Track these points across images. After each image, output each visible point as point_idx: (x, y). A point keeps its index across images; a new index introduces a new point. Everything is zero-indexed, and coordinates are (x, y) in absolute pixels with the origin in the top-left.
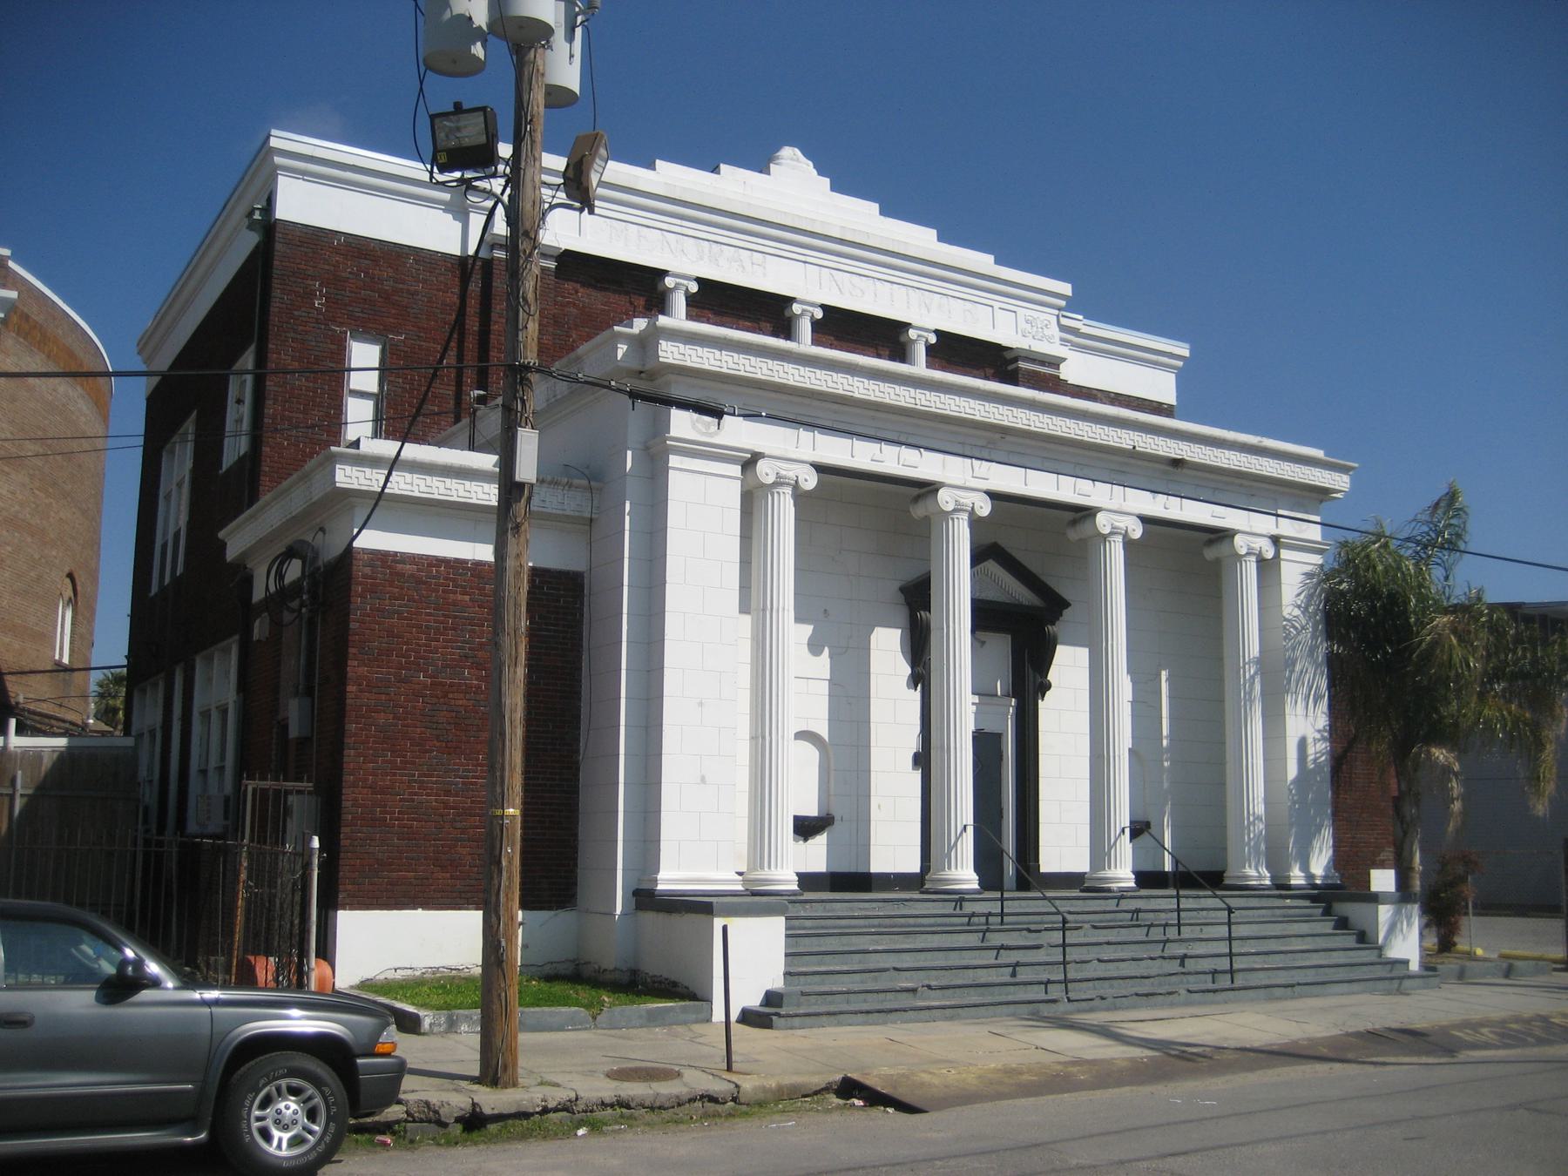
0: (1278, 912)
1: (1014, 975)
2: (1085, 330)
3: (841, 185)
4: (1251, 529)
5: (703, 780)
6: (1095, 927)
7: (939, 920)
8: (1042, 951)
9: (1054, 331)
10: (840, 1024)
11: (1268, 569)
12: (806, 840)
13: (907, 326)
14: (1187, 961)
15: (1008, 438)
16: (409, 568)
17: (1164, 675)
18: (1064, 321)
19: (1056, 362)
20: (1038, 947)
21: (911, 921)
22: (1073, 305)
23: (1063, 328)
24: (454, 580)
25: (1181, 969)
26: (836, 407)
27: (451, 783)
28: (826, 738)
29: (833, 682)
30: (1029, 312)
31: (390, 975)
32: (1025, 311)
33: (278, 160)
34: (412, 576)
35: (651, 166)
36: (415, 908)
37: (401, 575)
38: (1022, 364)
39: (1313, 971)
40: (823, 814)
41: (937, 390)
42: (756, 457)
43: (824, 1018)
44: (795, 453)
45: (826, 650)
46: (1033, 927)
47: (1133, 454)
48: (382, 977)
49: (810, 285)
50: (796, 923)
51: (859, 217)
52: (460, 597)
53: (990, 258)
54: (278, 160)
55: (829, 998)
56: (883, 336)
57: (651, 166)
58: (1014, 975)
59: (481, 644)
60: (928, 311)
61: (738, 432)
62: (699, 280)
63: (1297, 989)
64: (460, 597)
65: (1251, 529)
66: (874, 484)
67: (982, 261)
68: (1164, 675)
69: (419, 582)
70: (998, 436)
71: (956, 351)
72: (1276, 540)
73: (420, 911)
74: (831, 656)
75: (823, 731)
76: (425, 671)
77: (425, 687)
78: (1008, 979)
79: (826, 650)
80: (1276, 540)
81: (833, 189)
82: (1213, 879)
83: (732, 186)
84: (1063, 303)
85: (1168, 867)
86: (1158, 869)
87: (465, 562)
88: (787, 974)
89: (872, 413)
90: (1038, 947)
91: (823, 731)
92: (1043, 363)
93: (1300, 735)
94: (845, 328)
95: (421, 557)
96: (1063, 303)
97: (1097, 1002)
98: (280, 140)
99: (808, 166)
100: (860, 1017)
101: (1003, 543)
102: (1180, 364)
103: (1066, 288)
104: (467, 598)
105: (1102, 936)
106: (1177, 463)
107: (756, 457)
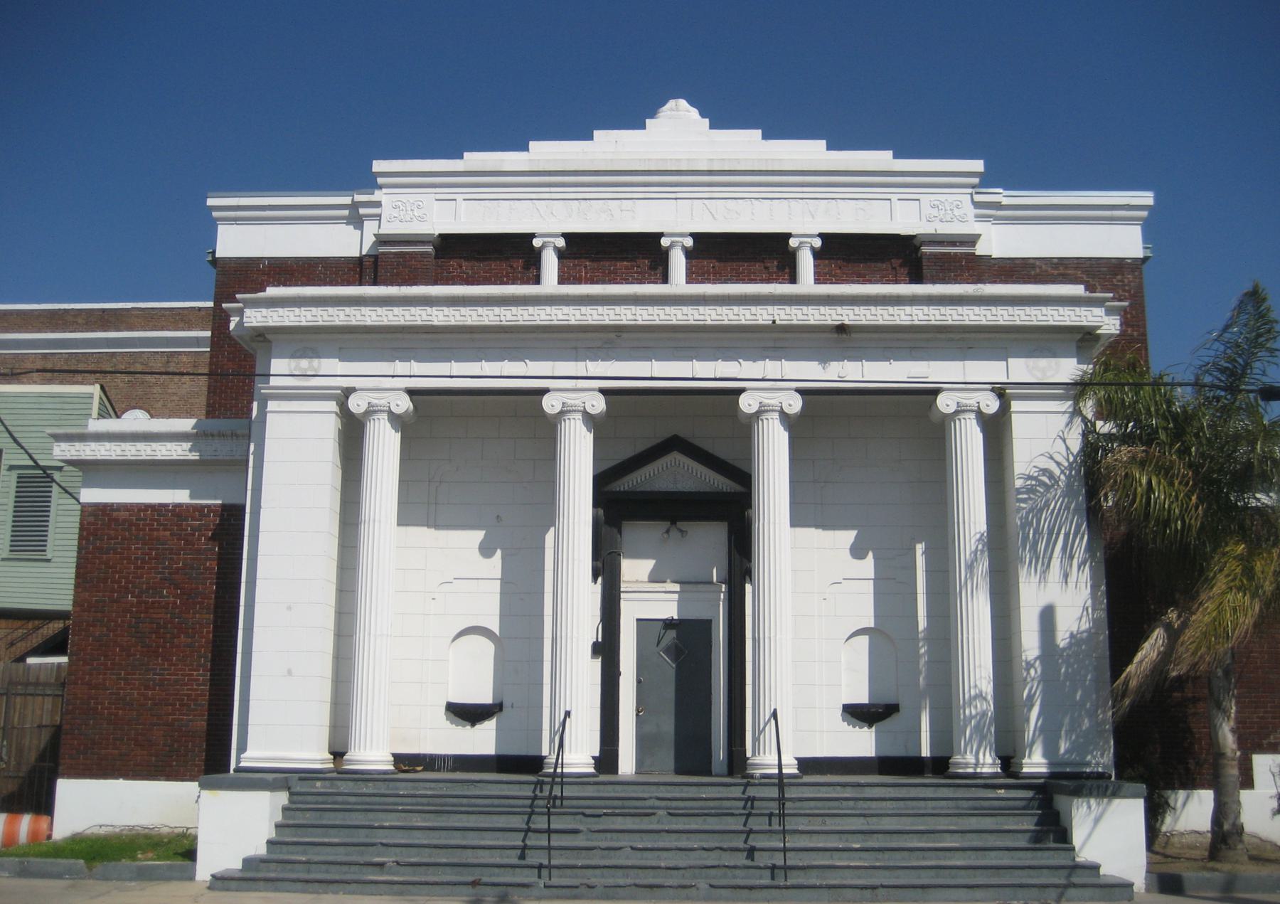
0: (965, 804)
1: (522, 857)
2: (1005, 201)
3: (718, 122)
4: (962, 383)
5: (290, 673)
6: (670, 814)
7: (496, 802)
8: (580, 836)
9: (971, 211)
10: (276, 890)
11: (996, 430)
12: (473, 725)
13: (789, 235)
14: (757, 854)
15: (625, 335)
16: (123, 515)
17: (920, 548)
18: (978, 198)
19: (972, 240)
20: (576, 832)
21: (465, 801)
22: (987, 180)
23: (977, 205)
24: (156, 520)
25: (749, 863)
26: (430, 336)
27: (149, 680)
28: (497, 631)
29: (504, 581)
30: (933, 197)
31: (96, 830)
32: (928, 197)
33: (215, 214)
34: (125, 520)
35: (525, 148)
36: (117, 778)
37: (116, 520)
38: (925, 249)
39: (932, 872)
40: (497, 702)
41: (525, 305)
42: (348, 392)
43: (262, 883)
44: (386, 385)
45: (499, 552)
46: (588, 811)
47: (774, 328)
48: (89, 832)
49: (676, 218)
50: (295, 798)
51: (745, 146)
52: (162, 533)
53: (889, 154)
54: (215, 214)
55: (289, 866)
56: (764, 254)
57: (525, 148)
58: (522, 857)
59: (178, 569)
60: (806, 219)
61: (333, 370)
62: (565, 235)
63: (881, 891)
64: (162, 533)
65: (962, 383)
66: (619, 397)
67: (881, 159)
68: (920, 548)
69: (131, 525)
70: (612, 335)
71: (848, 254)
72: (1001, 391)
73: (121, 781)
74: (503, 558)
75: (495, 627)
76: (133, 593)
77: (132, 606)
78: (515, 861)
79: (499, 552)
80: (1001, 391)
81: (712, 127)
82: (940, 765)
83: (610, 147)
84: (976, 180)
85: (925, 752)
86: (912, 753)
87: (166, 505)
88: (270, 843)
89: (468, 336)
90: (576, 832)
91: (495, 627)
92: (953, 244)
93: (1043, 602)
94: (723, 254)
95: (132, 505)
96: (976, 180)
97: (583, 890)
98: (211, 202)
99: (694, 113)
100: (299, 885)
101: (684, 433)
102: (1145, 214)
103: (978, 165)
104: (168, 533)
105: (680, 824)
106: (842, 329)
107: (348, 392)
